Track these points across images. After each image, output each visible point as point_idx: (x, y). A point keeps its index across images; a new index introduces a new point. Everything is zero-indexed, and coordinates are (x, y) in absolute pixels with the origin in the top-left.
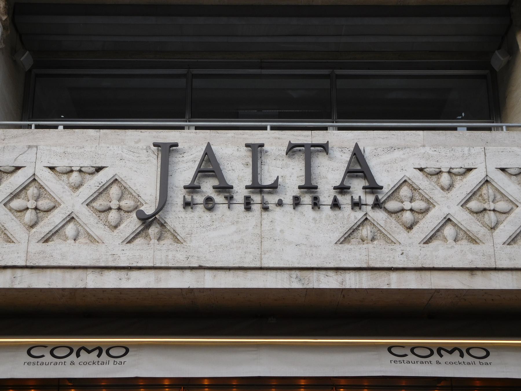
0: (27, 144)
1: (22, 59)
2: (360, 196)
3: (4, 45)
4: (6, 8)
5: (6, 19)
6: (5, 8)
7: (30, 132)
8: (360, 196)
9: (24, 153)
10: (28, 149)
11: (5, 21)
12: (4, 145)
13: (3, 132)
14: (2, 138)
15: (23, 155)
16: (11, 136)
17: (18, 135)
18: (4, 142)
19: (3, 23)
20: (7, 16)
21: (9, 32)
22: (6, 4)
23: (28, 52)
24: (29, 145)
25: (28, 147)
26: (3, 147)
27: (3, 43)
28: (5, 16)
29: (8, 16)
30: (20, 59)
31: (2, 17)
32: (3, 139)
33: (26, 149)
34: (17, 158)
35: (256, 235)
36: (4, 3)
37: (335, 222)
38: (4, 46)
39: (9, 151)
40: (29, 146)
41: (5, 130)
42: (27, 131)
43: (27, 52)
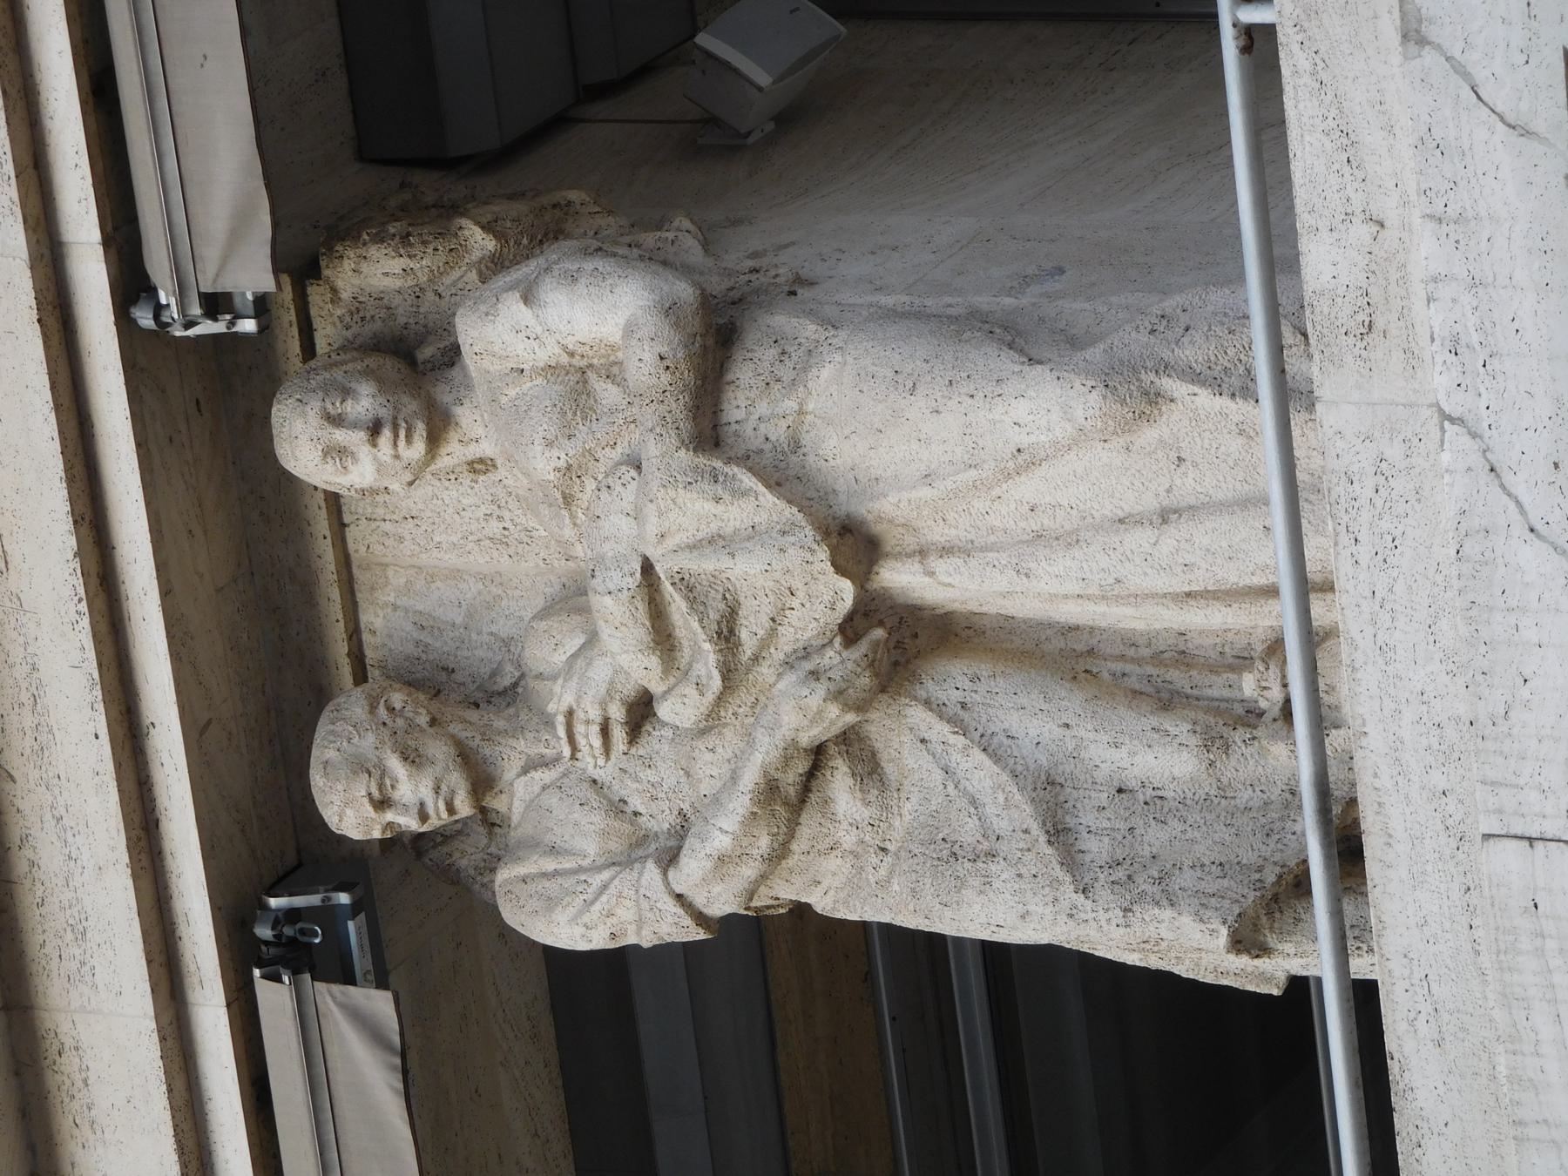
0: (1396, 59)
1: (763, 79)
2: (796, 295)
3: (676, 223)
4: (409, 234)
5: (483, 228)
6: (405, 239)
7: (1300, 37)
8: (796, 295)
9: (1465, 75)
10: (1429, 43)
11: (499, 236)
12: (1417, 221)
13: (1324, 233)
14: (1368, 239)
15: (1480, 75)
16: (1346, 169)
17: (1333, 124)
18: (1392, 218)
19: (517, 243)
20: (465, 222)
21: (574, 195)
22: (379, 239)
23: (703, 39)
24: (1397, 39)
25: (1413, 48)
26: (1431, 225)
27: (659, 227)
28: (466, 233)
29: (462, 215)
30: (760, 89)
31: (476, 255)
32: (1375, 228)
33: (1429, 57)
34: (1511, 119)
35: (1313, 179)
36: (374, 251)
37: (972, 387)
38: (687, 224)
39: (1462, 184)
40: (1405, 36)
41: (1304, 219)
42: (1293, 61)
43: (703, 39)
